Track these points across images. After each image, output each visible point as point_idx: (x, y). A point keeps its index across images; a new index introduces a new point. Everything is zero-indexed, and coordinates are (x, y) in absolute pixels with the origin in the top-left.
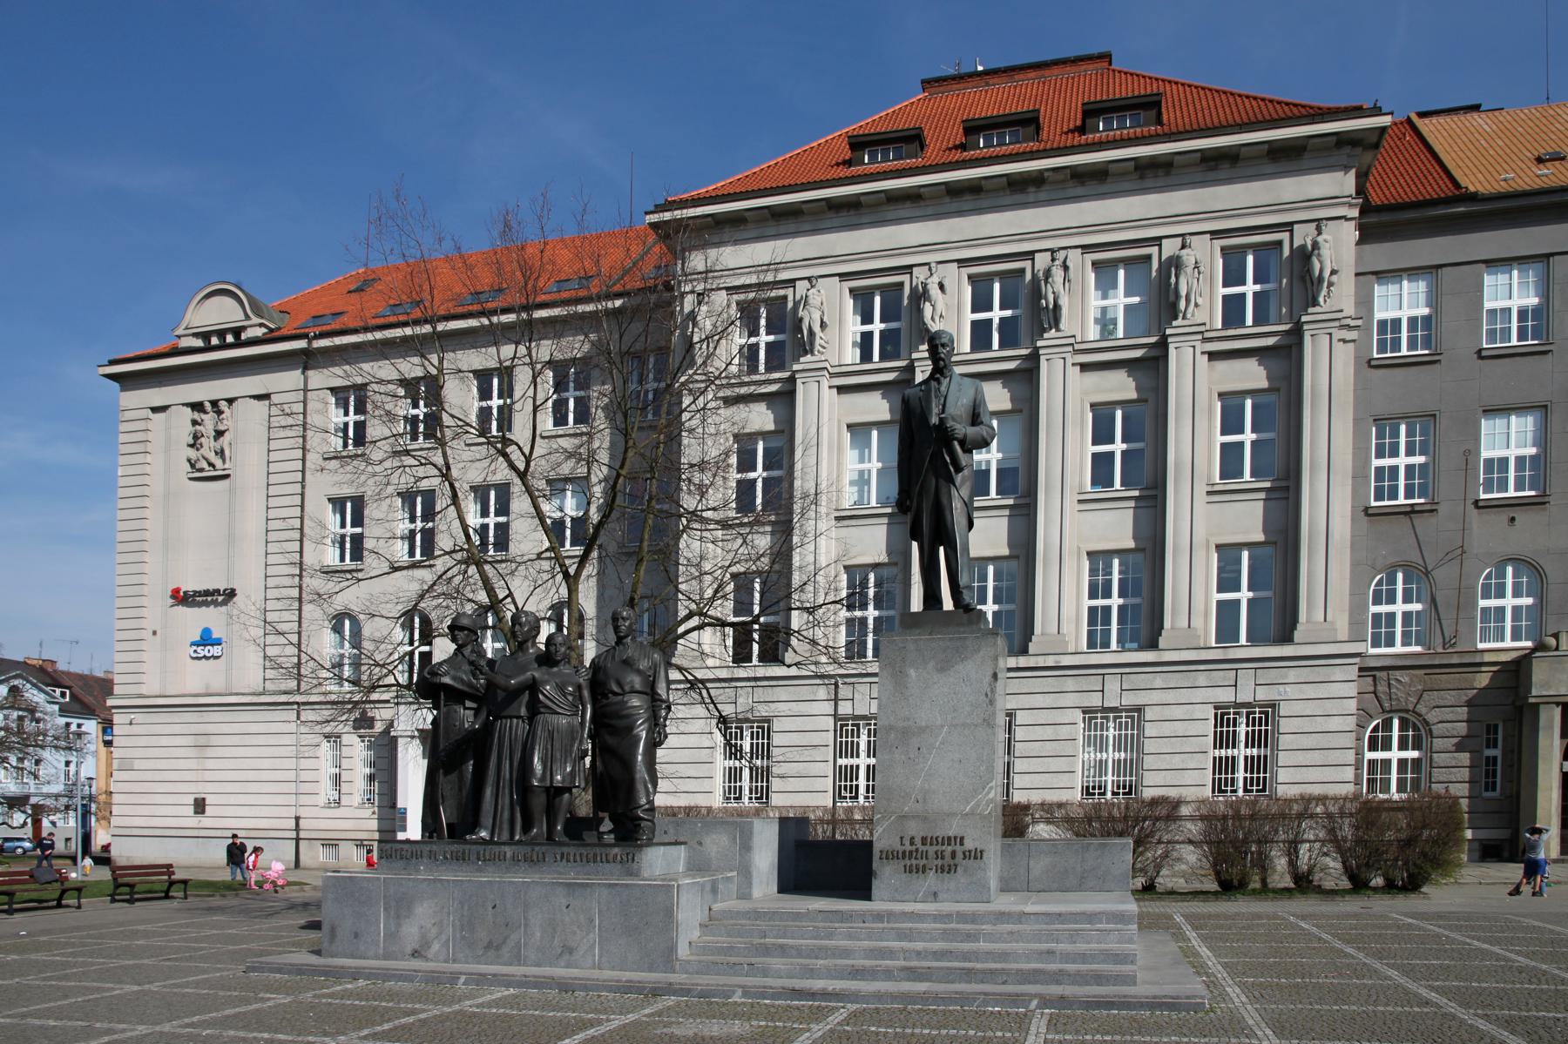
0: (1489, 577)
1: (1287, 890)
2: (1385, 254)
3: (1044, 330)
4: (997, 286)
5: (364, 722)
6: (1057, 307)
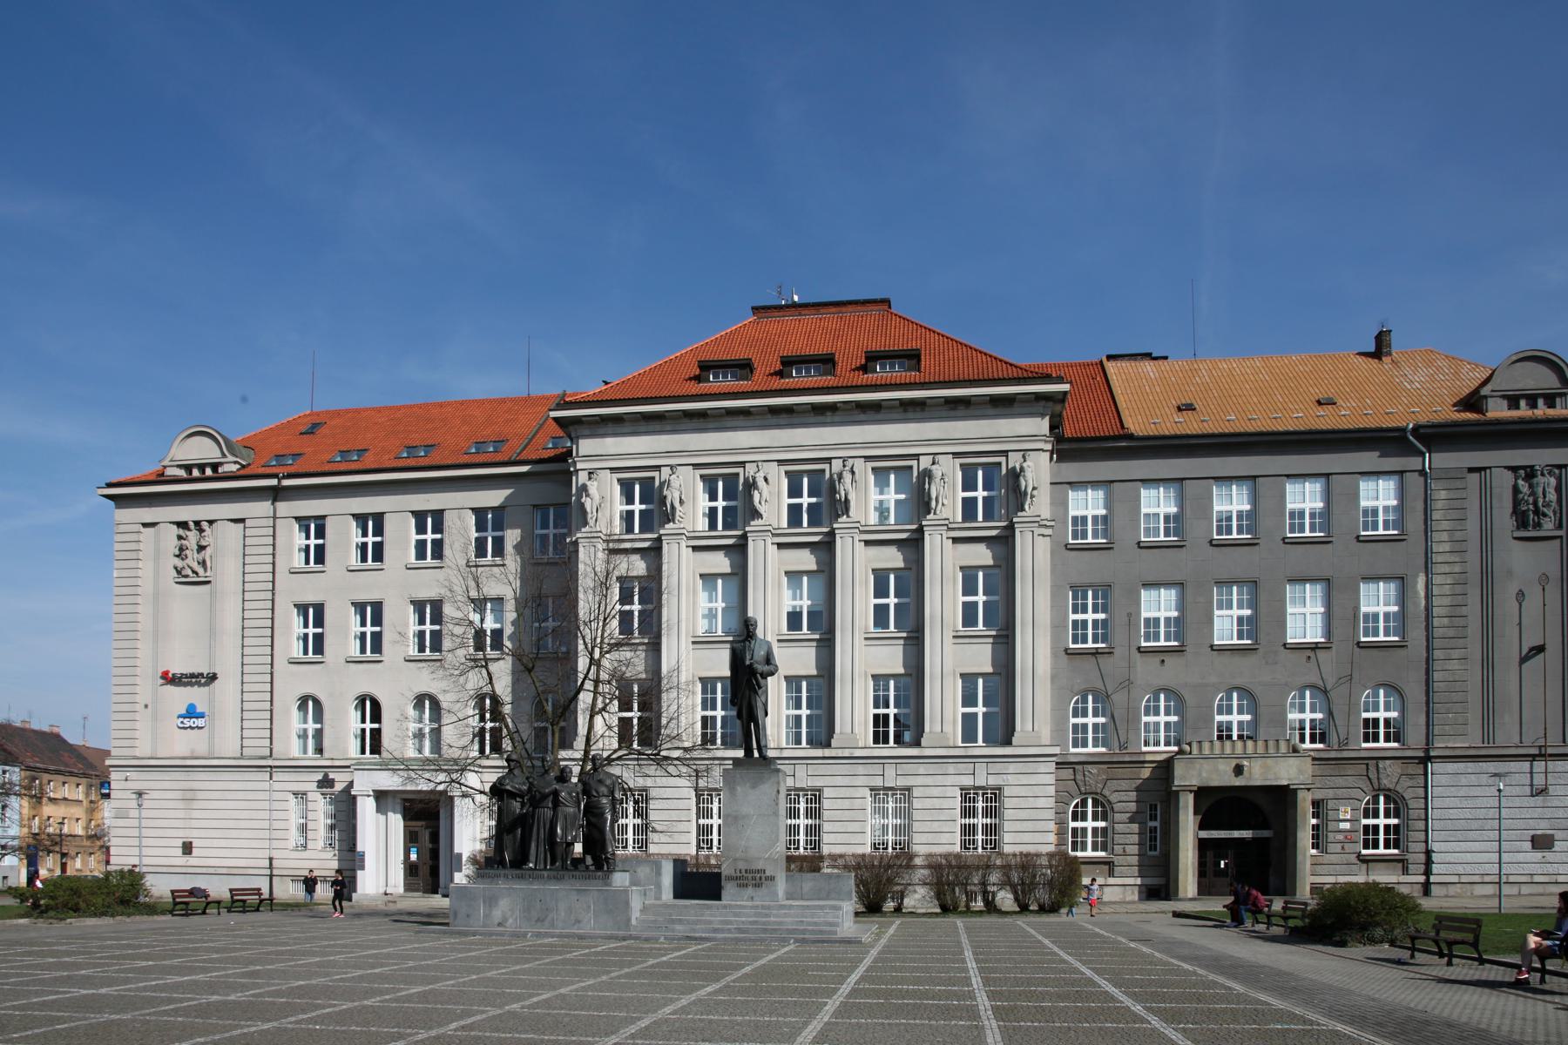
2: (1073, 470)
5: (326, 783)
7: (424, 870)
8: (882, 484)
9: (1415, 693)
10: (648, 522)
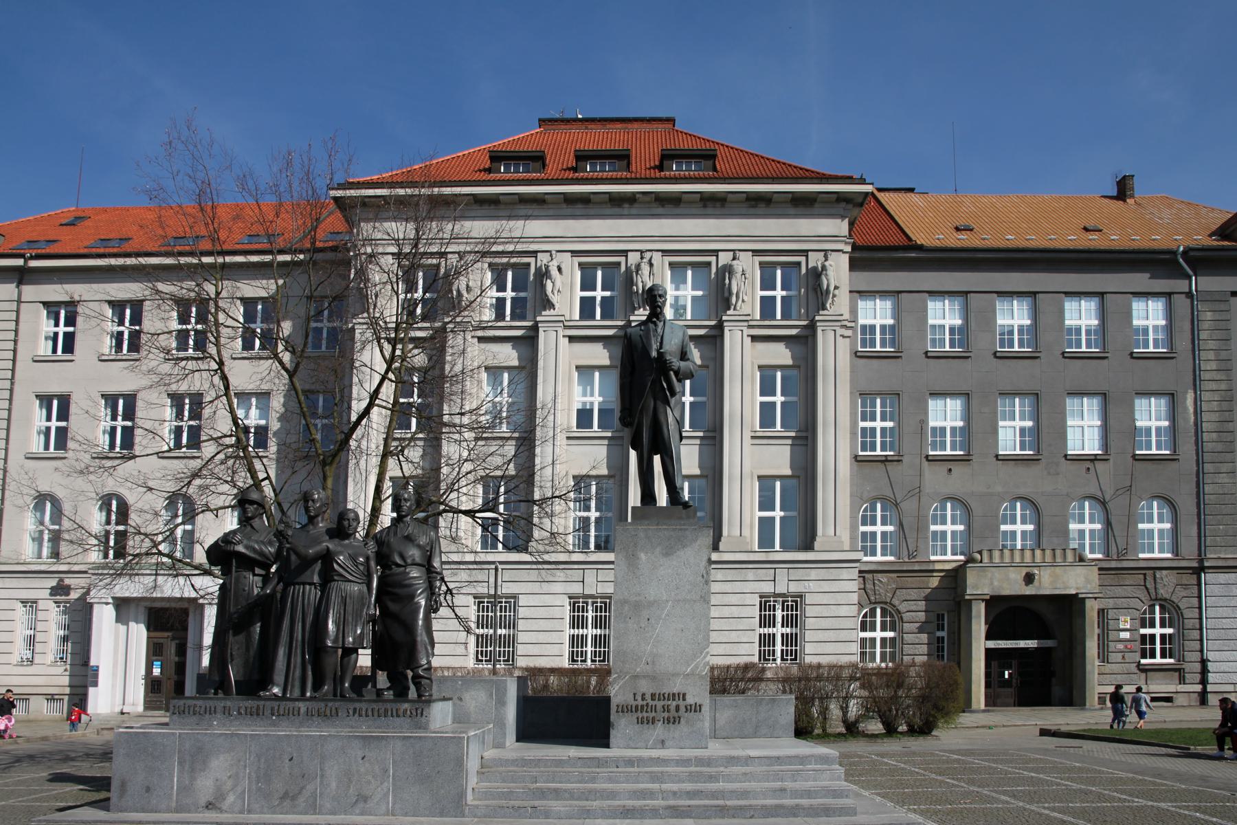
0: (936, 509)
1: (840, 735)
3: (635, 309)
4: (599, 273)
7: (168, 686)
8: (679, 281)
9: (1187, 505)
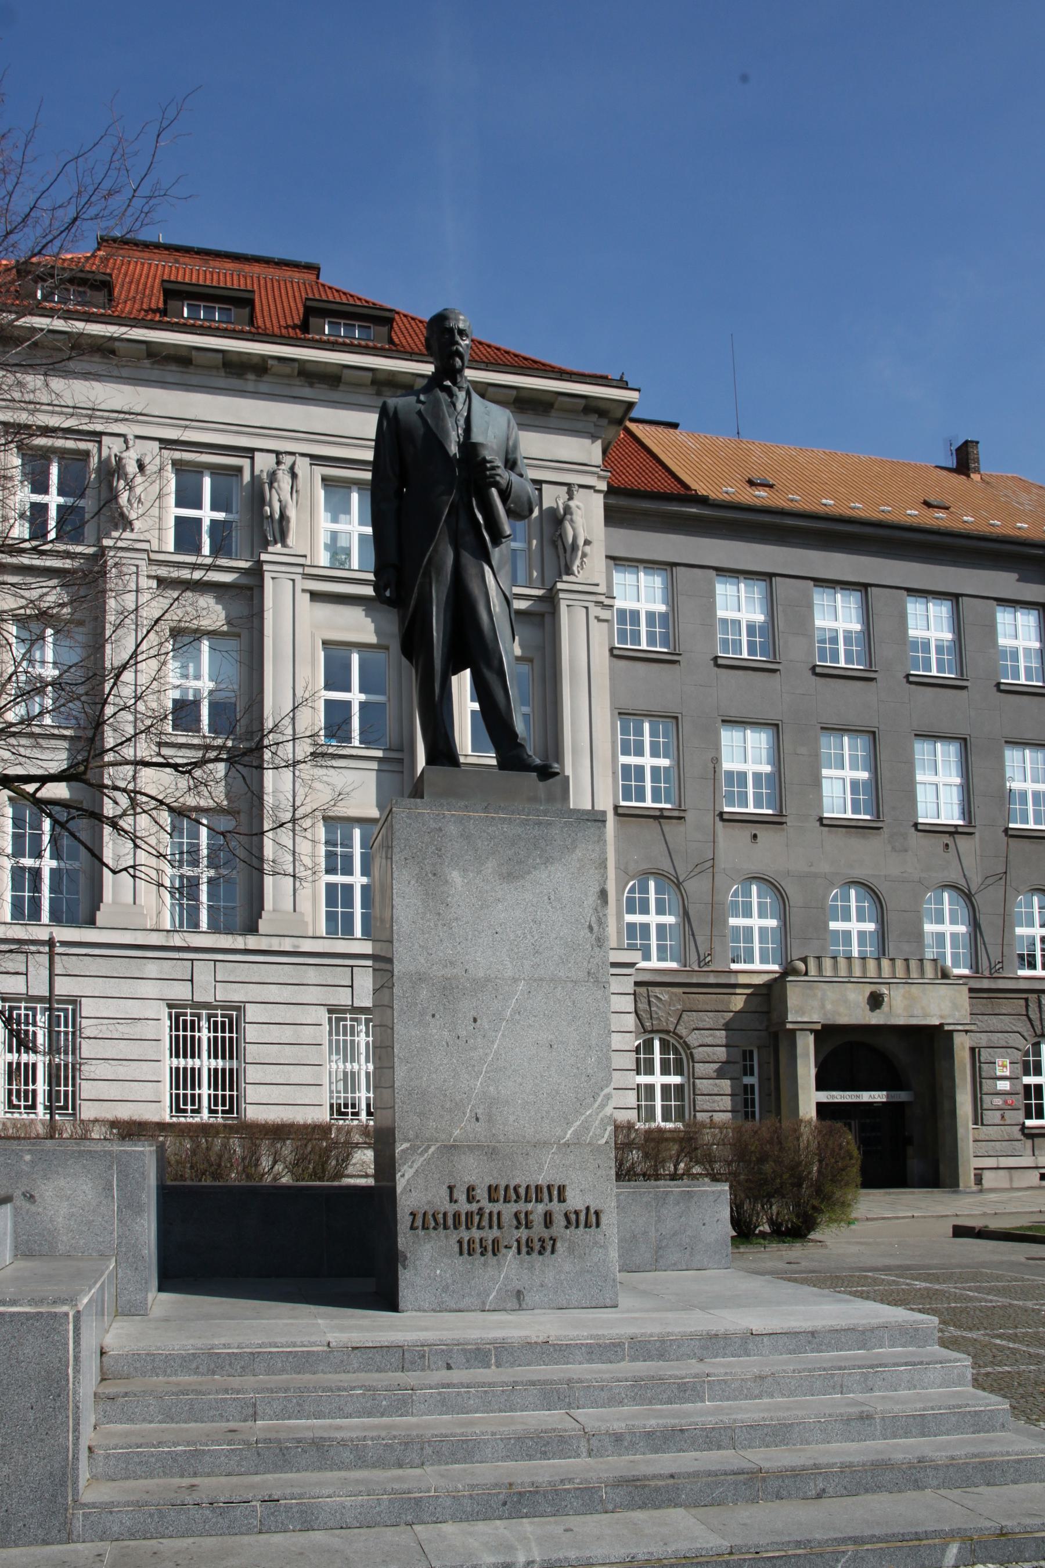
6: (283, 515)
8: (338, 509)
10: (71, 523)
